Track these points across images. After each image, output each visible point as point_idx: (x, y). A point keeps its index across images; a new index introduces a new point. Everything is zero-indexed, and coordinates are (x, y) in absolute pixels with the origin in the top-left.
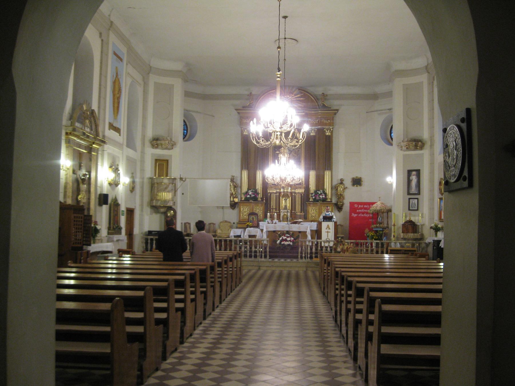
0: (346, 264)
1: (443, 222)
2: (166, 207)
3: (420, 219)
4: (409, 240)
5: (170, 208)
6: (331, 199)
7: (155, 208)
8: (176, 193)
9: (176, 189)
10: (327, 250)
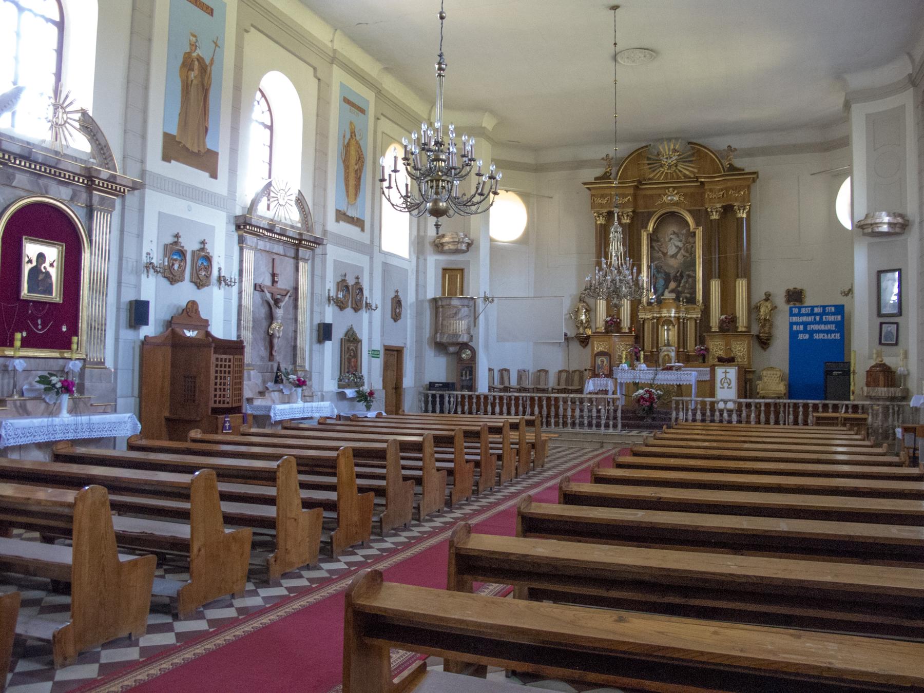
0: (807, 438)
2: (458, 344)
4: (878, 399)
5: (465, 346)
6: (749, 327)
7: (441, 347)
9: (477, 316)
10: (721, 415)
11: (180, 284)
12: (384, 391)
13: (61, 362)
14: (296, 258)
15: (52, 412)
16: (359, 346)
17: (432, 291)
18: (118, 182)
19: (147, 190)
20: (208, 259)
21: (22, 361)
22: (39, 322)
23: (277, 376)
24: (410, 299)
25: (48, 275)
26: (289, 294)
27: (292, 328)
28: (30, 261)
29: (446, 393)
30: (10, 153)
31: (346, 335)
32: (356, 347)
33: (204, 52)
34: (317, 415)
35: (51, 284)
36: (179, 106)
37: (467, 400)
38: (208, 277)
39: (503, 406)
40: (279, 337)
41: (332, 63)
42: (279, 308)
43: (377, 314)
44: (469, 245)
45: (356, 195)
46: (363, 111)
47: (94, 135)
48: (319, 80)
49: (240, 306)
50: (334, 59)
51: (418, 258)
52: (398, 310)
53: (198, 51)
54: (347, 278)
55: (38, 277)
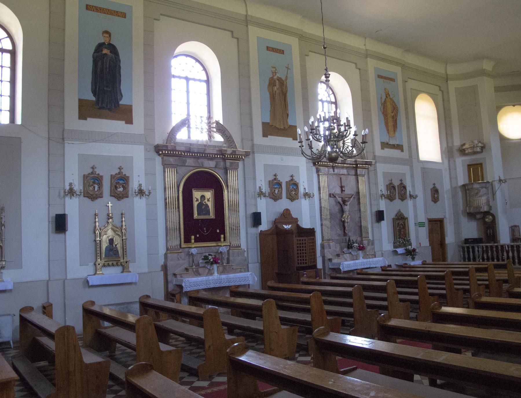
1: (419, 222)
2: (481, 212)
3: (132, 367)
5: (487, 213)
7: (471, 215)
8: (495, 196)
9: (494, 193)
11: (280, 200)
12: (430, 247)
13: (217, 247)
14: (356, 175)
15: (210, 273)
16: (406, 222)
17: (462, 179)
18: (237, 153)
19: (256, 154)
20: (296, 185)
21: (195, 249)
22: (205, 229)
23: (348, 245)
24: (445, 187)
25: (207, 206)
26: (353, 197)
27: (357, 216)
28: (197, 200)
29: (475, 245)
30: (181, 151)
31: (396, 215)
32: (404, 222)
33: (281, 74)
34: (379, 265)
35: (209, 210)
36: (270, 106)
37: (489, 249)
38: (297, 194)
39: (468, 257)
40: (347, 222)
41: (367, 57)
42: (346, 205)
43: (420, 200)
44: (482, 148)
45: (395, 131)
46: (393, 80)
47: (224, 132)
48: (359, 69)
49: (321, 207)
50: (367, 55)
51: (449, 161)
52: (436, 196)
53: (278, 75)
54: (393, 182)
55: (202, 207)
